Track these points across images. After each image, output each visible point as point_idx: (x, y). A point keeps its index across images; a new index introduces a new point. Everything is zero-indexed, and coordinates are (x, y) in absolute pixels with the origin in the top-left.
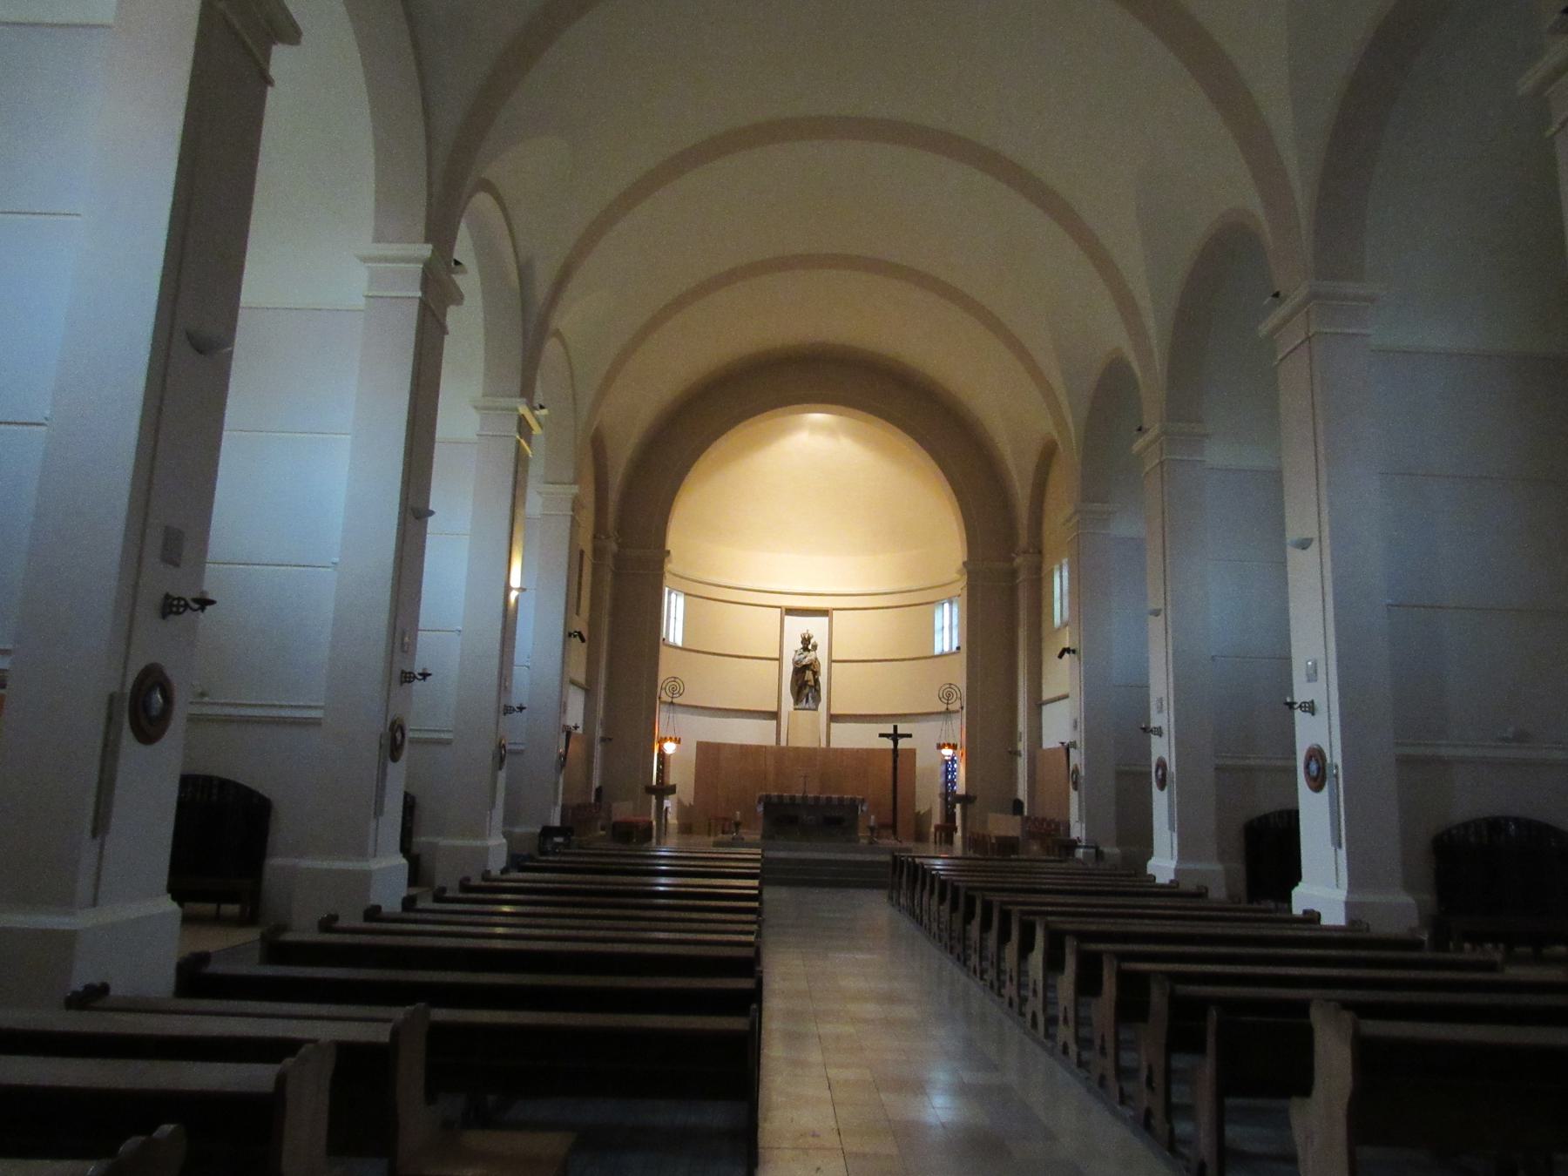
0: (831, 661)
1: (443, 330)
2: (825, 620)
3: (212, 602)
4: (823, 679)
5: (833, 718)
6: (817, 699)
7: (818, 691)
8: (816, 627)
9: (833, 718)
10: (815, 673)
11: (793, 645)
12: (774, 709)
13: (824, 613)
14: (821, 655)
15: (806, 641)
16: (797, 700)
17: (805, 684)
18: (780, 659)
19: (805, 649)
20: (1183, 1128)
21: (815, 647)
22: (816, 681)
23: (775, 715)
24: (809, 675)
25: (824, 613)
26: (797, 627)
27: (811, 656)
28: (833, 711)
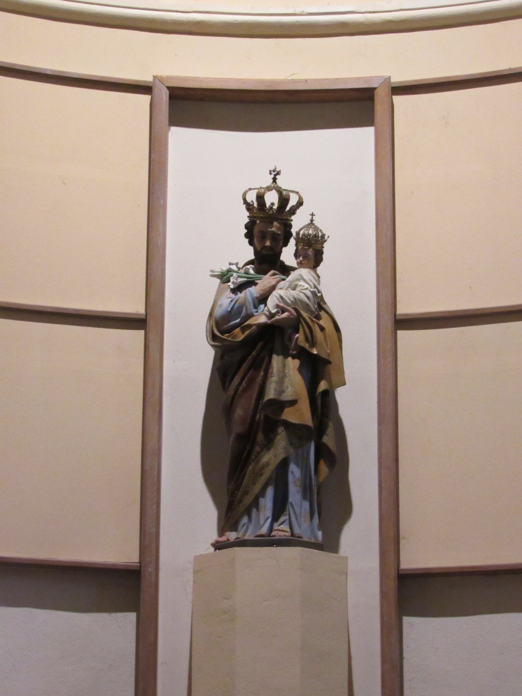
0: (397, 322)
1: (247, 226)
2: (360, 140)
3: (313, 213)
4: (356, 404)
5: (414, 591)
6: (331, 506)
7: (334, 457)
8: (323, 171)
9: (414, 591)
10: (319, 368)
11: (208, 244)
12: (123, 552)
13: (350, 106)
14: (345, 286)
15: (270, 226)
16: (232, 510)
17: (268, 418)
18: (143, 323)
19: (267, 260)
20: (321, 322)
21: (312, 250)
22: (324, 407)
23: (125, 587)
24: (286, 377)
25: (350, 106)
26: (219, 172)
27: (286, 292)
28: (415, 557)
